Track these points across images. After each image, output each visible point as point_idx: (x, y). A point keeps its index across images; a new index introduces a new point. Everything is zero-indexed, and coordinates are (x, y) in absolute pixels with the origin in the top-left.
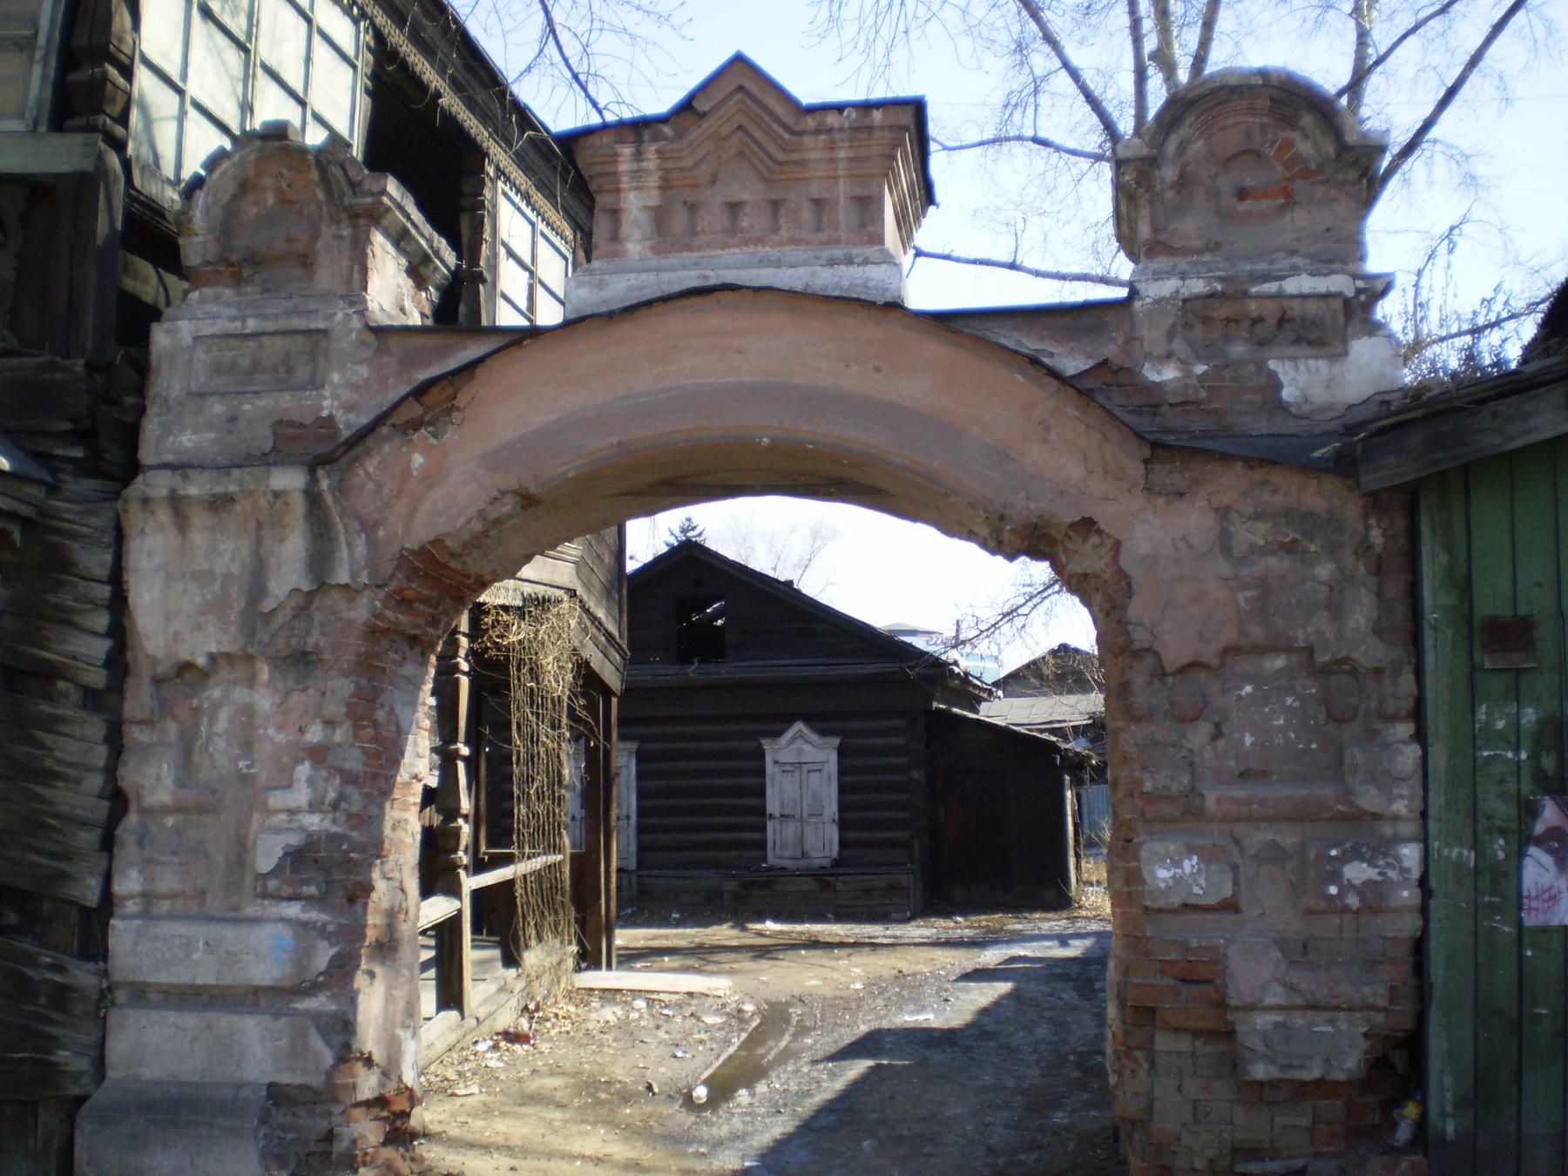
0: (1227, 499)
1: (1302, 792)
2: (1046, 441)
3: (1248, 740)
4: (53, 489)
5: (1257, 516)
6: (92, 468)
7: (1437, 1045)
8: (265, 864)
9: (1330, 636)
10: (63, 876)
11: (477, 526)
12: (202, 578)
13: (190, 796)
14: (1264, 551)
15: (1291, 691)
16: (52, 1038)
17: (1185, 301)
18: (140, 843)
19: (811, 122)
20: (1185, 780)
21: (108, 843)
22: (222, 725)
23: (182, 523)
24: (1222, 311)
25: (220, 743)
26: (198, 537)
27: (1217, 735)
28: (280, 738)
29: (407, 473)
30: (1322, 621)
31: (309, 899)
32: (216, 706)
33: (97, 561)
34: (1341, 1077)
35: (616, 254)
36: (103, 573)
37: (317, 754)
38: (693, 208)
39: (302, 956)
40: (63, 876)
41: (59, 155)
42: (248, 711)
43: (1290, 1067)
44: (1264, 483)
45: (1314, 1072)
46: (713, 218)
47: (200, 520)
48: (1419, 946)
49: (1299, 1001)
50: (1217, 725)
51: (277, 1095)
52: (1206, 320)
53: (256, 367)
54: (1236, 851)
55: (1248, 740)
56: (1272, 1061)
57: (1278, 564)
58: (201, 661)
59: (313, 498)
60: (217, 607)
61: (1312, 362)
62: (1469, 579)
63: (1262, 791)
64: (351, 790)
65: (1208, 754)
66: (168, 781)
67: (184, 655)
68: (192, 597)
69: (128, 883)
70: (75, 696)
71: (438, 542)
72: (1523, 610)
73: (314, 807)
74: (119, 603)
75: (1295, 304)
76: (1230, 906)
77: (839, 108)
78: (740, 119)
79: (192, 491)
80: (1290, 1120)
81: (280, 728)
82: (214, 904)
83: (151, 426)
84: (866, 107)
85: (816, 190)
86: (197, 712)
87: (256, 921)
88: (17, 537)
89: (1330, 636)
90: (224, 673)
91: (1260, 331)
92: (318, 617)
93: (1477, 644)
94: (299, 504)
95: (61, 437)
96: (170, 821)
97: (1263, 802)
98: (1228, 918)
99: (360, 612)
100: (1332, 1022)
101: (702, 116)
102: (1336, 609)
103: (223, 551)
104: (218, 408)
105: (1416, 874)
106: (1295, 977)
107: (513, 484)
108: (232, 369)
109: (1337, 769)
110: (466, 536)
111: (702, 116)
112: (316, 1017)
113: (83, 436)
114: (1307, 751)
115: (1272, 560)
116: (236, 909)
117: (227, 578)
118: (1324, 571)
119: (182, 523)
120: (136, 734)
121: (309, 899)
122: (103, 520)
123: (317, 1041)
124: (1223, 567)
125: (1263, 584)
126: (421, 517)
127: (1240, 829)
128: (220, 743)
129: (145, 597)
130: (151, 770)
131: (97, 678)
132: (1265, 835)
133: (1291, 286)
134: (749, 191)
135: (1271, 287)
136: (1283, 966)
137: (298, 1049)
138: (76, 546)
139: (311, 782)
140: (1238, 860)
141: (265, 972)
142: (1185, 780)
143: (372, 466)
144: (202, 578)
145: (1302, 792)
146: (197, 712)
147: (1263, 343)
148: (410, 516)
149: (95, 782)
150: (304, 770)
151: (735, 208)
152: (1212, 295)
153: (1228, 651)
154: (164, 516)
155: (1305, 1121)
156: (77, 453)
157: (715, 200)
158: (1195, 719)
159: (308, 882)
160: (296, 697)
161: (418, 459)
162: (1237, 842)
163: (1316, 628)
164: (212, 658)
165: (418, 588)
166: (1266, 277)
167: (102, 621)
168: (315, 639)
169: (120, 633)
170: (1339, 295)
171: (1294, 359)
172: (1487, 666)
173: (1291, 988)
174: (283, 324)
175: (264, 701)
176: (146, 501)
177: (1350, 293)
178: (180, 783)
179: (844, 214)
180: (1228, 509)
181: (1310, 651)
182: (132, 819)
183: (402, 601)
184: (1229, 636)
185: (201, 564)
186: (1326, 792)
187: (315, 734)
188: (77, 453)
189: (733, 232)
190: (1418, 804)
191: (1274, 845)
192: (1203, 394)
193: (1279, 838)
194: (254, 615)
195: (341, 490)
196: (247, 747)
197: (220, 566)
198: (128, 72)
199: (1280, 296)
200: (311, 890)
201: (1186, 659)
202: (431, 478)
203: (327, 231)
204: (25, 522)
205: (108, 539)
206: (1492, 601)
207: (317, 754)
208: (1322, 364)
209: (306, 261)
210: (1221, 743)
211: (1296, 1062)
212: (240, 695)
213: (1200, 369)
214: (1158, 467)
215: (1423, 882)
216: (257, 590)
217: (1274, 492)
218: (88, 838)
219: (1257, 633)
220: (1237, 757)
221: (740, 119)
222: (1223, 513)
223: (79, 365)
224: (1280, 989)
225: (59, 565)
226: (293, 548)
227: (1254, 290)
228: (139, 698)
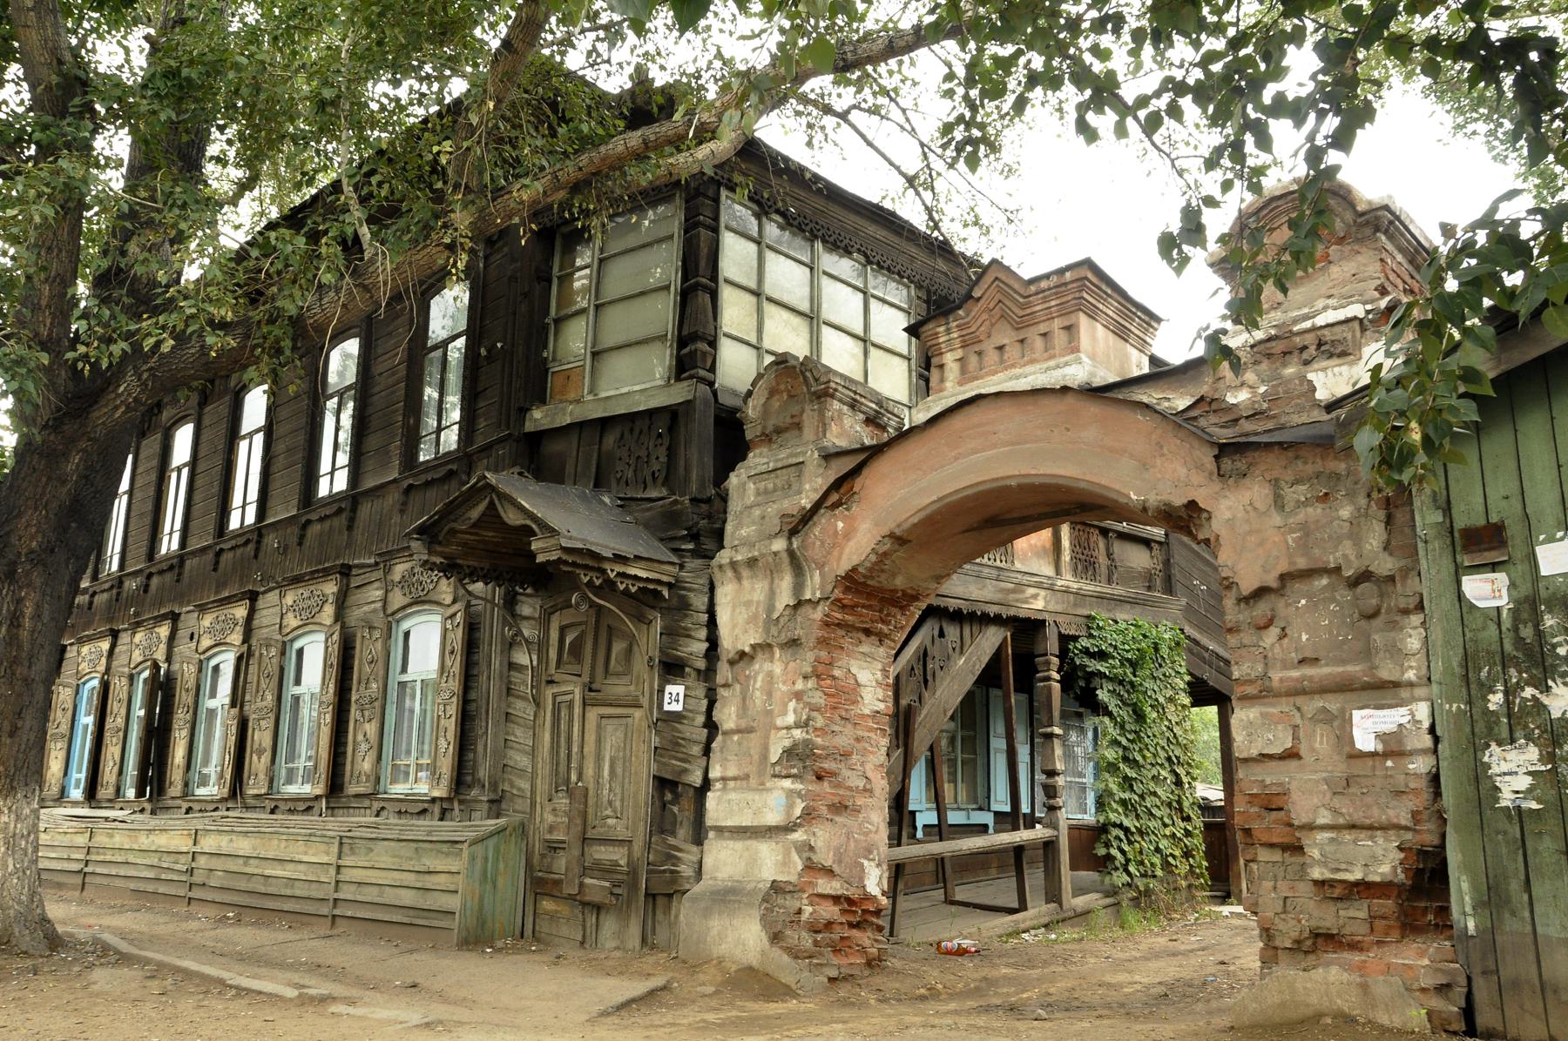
0: (1275, 474)
1: (1340, 669)
2: (1163, 455)
3: (1304, 637)
4: (682, 567)
5: (1296, 482)
6: (696, 554)
7: (1454, 857)
8: (774, 758)
9: (1352, 558)
10: (686, 771)
11: (873, 558)
12: (748, 604)
13: (743, 724)
14: (1306, 503)
15: (1333, 600)
16: (679, 859)
17: (1252, 347)
18: (722, 751)
19: (1033, 288)
20: (1260, 668)
21: (707, 751)
22: (758, 684)
23: (739, 578)
24: (1278, 347)
25: (758, 693)
26: (746, 583)
27: (1283, 635)
28: (784, 688)
29: (836, 532)
30: (1347, 548)
31: (794, 776)
32: (757, 673)
33: (699, 602)
34: (1377, 879)
35: (941, 390)
36: (704, 608)
37: (798, 696)
38: (979, 353)
39: (790, 807)
40: (686, 771)
41: (679, 393)
42: (770, 675)
43: (1338, 870)
44: (1297, 457)
45: (1356, 875)
46: (992, 357)
47: (745, 573)
48: (1435, 779)
49: (1341, 821)
50: (1283, 629)
51: (777, 888)
52: (1269, 356)
53: (775, 490)
54: (1298, 715)
55: (1304, 637)
56: (1324, 864)
57: (1315, 512)
58: (747, 649)
59: (791, 553)
60: (753, 619)
61: (1336, 370)
62: (1449, 502)
63: (1309, 671)
64: (814, 714)
65: (1277, 649)
66: (733, 716)
67: (740, 647)
68: (743, 615)
69: (715, 773)
70: (694, 674)
71: (854, 569)
72: (1494, 519)
73: (797, 726)
74: (712, 623)
75: (1326, 332)
76: (1291, 755)
77: (1047, 276)
78: (999, 296)
79: (739, 558)
80: (1352, 913)
81: (784, 683)
82: (753, 782)
83: (729, 528)
84: (1061, 272)
85: (1043, 328)
86: (748, 677)
87: (768, 790)
88: (666, 593)
89: (1352, 558)
90: (760, 656)
91: (1305, 356)
92: (799, 619)
93: (1458, 549)
94: (785, 556)
95: (683, 538)
96: (736, 738)
97: (1311, 679)
98: (1293, 764)
99: (818, 614)
100: (1372, 838)
101: (979, 299)
102: (1356, 538)
103: (756, 589)
104: (757, 512)
105: (1426, 724)
106: (1336, 802)
107: (886, 531)
108: (766, 492)
109: (1367, 653)
110: (868, 564)
111: (979, 299)
112: (795, 843)
113: (694, 537)
114: (1345, 641)
115: (1310, 510)
116: (763, 784)
117: (758, 602)
118: (1346, 512)
119: (739, 578)
120: (722, 692)
121: (794, 776)
122: (704, 581)
123: (795, 857)
124: (1277, 519)
125: (1304, 528)
126: (845, 557)
127: (1299, 700)
128: (758, 693)
129: (723, 617)
130: (726, 711)
131: (701, 664)
132: (1318, 703)
133: (1320, 321)
134: (1005, 336)
135: (1307, 324)
136: (1328, 795)
137: (786, 863)
138: (691, 595)
139: (795, 711)
140: (1299, 721)
141: (773, 818)
142: (1260, 668)
143: (817, 530)
144: (748, 604)
145: (1340, 669)
146: (748, 677)
147: (1307, 363)
148: (840, 558)
149: (701, 719)
150: (792, 705)
151: (1001, 348)
152: (1269, 339)
153: (1283, 577)
154: (730, 573)
155: (1363, 914)
156: (690, 546)
157: (989, 346)
158: (1266, 627)
159: (793, 767)
160: (792, 664)
161: (840, 525)
162: (1299, 709)
163: (1345, 555)
164: (753, 647)
165: (848, 599)
166: (1306, 317)
167: (703, 634)
168: (799, 632)
169: (713, 642)
170: (1355, 318)
171: (1324, 370)
172: (1467, 564)
173: (1335, 811)
174: (786, 463)
175: (777, 668)
176: (720, 567)
177: (1361, 315)
178: (739, 717)
179: (1060, 338)
180: (1277, 480)
181: (1338, 569)
182: (719, 738)
183: (840, 605)
184: (1283, 567)
185: (748, 597)
186: (1354, 669)
187: (800, 685)
188: (690, 546)
189: (1004, 365)
190: (1424, 671)
191: (1324, 710)
192: (1265, 405)
193: (1327, 705)
194: (771, 622)
195: (803, 546)
196: (770, 694)
197: (756, 598)
198: (713, 344)
199: (1314, 329)
200: (795, 771)
201: (1256, 585)
202: (848, 535)
203: (808, 408)
204: (670, 585)
205: (706, 589)
206: (1468, 514)
207: (798, 696)
208: (1344, 369)
209: (798, 426)
210: (1286, 640)
211: (1343, 866)
212: (767, 666)
213: (1262, 389)
214: (1225, 460)
215: (1432, 730)
216: (770, 608)
217: (1305, 463)
218: (696, 750)
219: (1302, 563)
220: (1296, 650)
221: (999, 296)
222: (1275, 483)
223: (686, 500)
224: (1326, 813)
225: (684, 606)
226: (786, 583)
227: (1295, 329)
228: (724, 672)
